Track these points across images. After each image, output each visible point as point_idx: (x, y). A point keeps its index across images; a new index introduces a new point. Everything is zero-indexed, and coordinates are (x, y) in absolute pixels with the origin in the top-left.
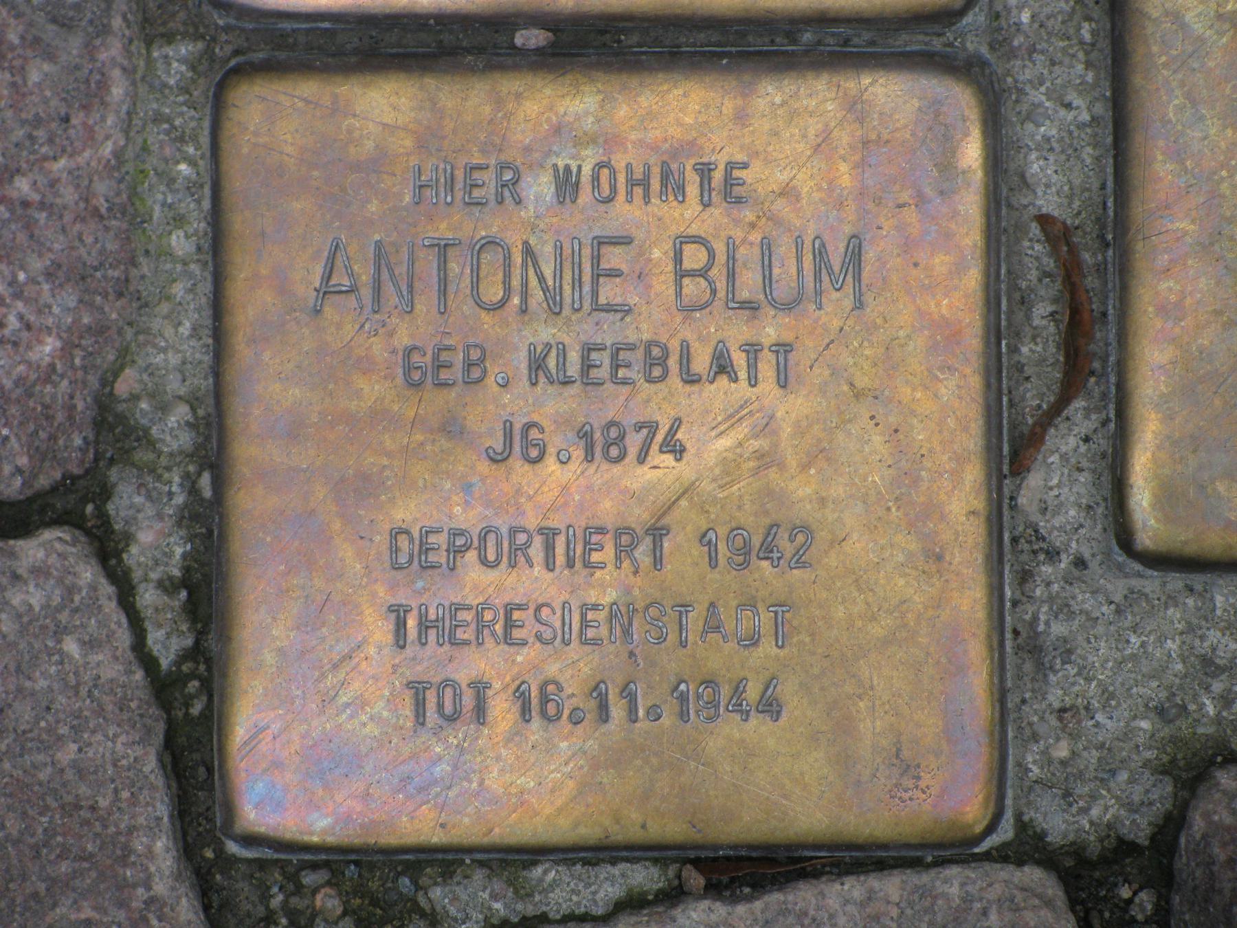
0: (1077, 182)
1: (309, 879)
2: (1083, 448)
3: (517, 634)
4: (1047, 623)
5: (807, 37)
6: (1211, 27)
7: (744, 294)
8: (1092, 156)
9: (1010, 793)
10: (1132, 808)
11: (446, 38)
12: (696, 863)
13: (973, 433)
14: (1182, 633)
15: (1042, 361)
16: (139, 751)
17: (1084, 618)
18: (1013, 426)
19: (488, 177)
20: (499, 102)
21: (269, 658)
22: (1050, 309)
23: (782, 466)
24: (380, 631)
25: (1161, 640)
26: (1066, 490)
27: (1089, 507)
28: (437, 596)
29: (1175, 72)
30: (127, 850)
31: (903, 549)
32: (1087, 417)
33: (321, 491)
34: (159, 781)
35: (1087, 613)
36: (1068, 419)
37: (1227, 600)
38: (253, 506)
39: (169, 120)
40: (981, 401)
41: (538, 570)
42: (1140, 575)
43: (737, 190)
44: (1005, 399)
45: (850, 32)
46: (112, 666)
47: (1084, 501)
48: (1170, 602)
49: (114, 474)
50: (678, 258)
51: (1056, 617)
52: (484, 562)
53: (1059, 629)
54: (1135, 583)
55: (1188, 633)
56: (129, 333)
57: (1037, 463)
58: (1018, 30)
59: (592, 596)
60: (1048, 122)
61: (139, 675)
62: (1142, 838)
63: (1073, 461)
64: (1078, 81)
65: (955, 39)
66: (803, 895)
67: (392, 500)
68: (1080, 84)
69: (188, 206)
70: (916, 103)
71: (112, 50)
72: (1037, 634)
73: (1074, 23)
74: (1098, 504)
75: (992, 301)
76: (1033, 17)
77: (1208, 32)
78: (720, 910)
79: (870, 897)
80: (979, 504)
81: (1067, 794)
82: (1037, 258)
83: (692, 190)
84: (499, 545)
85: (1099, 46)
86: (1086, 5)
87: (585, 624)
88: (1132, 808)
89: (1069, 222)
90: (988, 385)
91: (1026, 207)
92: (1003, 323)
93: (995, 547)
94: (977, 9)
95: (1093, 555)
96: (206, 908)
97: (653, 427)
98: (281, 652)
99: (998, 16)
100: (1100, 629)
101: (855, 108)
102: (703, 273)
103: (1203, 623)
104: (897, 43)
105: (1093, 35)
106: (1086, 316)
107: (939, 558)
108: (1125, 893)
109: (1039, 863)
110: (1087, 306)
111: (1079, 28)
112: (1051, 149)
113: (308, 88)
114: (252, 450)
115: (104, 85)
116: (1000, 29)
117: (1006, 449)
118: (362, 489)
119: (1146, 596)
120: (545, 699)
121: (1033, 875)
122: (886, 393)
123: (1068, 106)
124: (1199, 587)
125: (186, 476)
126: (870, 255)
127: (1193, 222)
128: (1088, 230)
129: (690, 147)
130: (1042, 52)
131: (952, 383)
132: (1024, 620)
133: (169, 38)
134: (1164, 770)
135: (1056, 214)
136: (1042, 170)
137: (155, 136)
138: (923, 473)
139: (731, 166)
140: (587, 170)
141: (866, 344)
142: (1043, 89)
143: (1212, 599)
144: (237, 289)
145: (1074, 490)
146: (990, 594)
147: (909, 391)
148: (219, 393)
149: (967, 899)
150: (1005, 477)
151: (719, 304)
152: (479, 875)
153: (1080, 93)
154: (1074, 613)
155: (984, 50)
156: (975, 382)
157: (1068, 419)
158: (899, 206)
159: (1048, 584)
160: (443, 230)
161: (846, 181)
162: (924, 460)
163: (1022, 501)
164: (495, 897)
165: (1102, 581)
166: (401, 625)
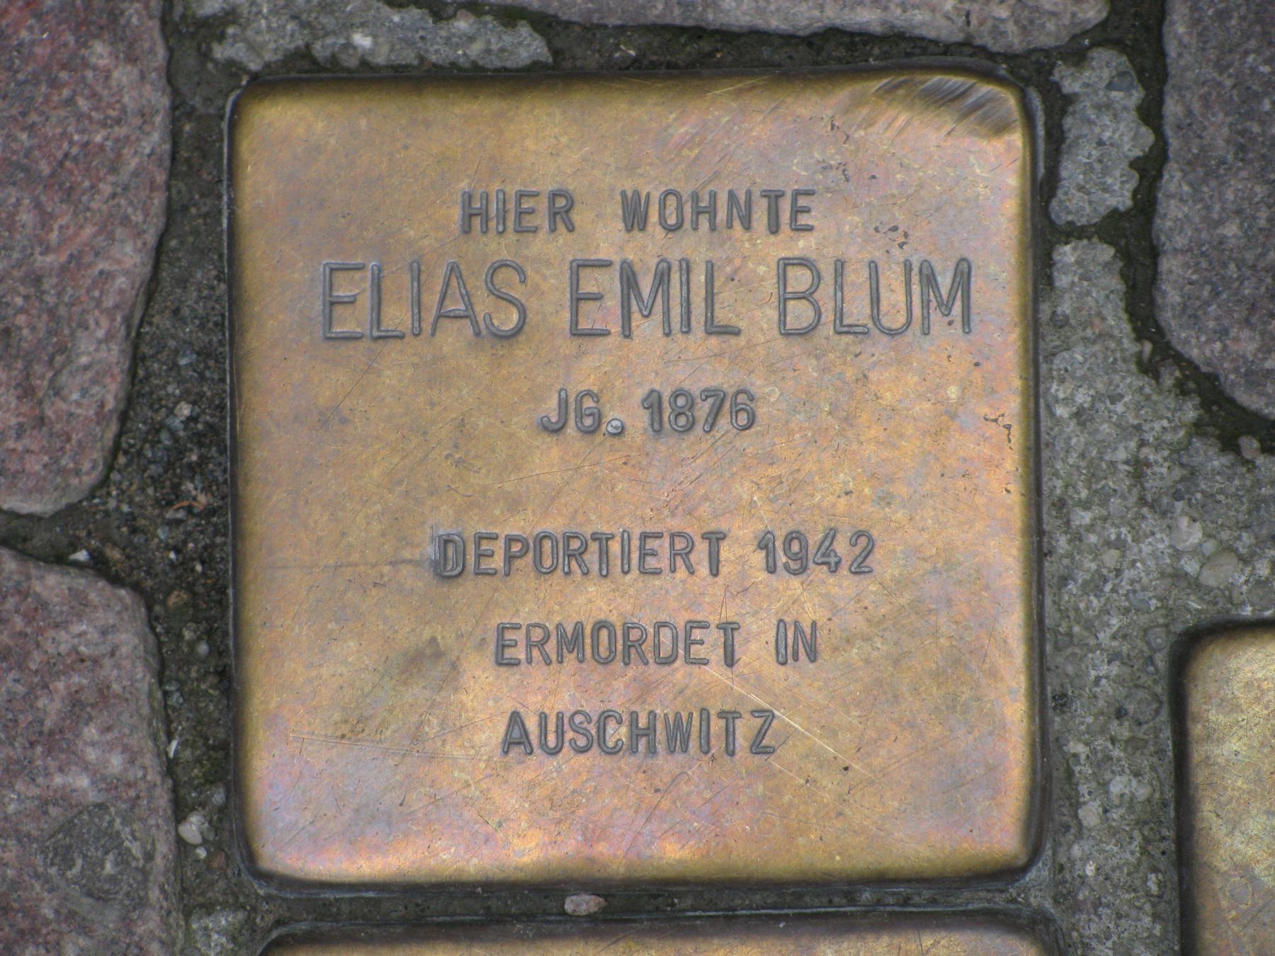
45: (909, 891)
58: (1083, 883)
64: (1145, 934)
65: (1019, 895)
68: (1148, 937)
73: (1141, 875)
94: (1040, 864)
99: (1061, 868)
104: (959, 901)
111: (1146, 880)
130: (1108, 906)
142: (1109, 944)
155: (1048, 904)
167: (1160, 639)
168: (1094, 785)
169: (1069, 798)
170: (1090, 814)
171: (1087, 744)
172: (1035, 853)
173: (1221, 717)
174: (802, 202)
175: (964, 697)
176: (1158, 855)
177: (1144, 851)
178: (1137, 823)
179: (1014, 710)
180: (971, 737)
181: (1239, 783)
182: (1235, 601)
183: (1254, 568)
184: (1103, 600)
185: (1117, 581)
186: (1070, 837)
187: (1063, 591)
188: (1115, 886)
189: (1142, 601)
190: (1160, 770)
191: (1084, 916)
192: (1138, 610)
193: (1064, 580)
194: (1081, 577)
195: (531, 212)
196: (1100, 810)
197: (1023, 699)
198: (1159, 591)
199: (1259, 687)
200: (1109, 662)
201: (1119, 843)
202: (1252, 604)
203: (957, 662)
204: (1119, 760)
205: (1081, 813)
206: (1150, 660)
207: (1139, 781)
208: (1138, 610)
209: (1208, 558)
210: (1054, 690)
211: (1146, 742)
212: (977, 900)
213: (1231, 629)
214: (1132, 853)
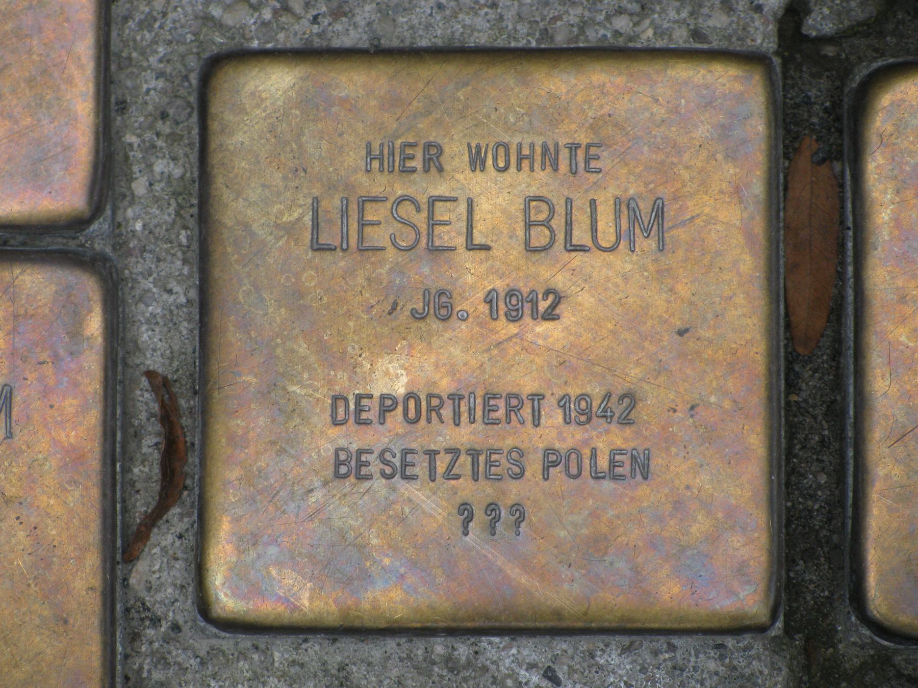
0: (176, 348)
2: (178, 543)
4: (149, 671)
6: (271, 234)
8: (187, 328)
13: (92, 530)
14: (249, 680)
15: (149, 478)
17: (177, 668)
18: (125, 526)
22: (155, 440)
26: (166, 573)
27: (182, 587)
29: (244, 266)
31: (40, 615)
32: (181, 520)
35: (179, 664)
36: (167, 521)
37: (283, 655)
40: (98, 506)
42: (216, 636)
44: (118, 506)
45: (7, 235)
47: (179, 582)
48: (241, 657)
51: (155, 667)
54: (214, 642)
55: (254, 680)
57: (144, 554)
58: (134, 236)
60: (154, 303)
63: (171, 552)
64: (177, 273)
65: (86, 242)
68: (179, 275)
70: (54, 287)
72: (142, 680)
73: (175, 231)
74: (189, 584)
76: (144, 226)
77: (269, 238)
80: (97, 582)
82: (146, 403)
85: (192, 248)
86: (184, 218)
89: (170, 377)
90: (104, 495)
91: (138, 366)
92: (118, 450)
93: (108, 613)
94: (101, 220)
95: (186, 622)
99: (119, 225)
100: (189, 676)
103: (265, 672)
104: (42, 244)
105: (188, 240)
106: (181, 446)
107: (66, 622)
110: (181, 438)
111: (178, 235)
112: (157, 323)
116: (121, 235)
117: (119, 543)
119: (223, 652)
122: (29, 500)
123: (170, 292)
124: (262, 646)
126: (18, 399)
127: (255, 376)
128: (184, 382)
130: (151, 252)
131: (77, 494)
132: (133, 670)
135: (160, 371)
136: (150, 338)
138: (55, 559)
141: (14, 464)
142: (151, 279)
143: (272, 655)
145: (172, 574)
146: (104, 649)
147: (45, 498)
150: (118, 563)
153: (179, 282)
154: (169, 664)
155: (108, 250)
156: (95, 492)
157: (167, 521)
158: (40, 363)
159: (151, 643)
162: (56, 550)
163: (133, 581)
165: (191, 641)
167: (193, 62)
168: (143, 165)
169: (126, 176)
170: (140, 187)
171: (139, 136)
172: (96, 210)
173: (231, 117)
174: (593, 151)
175: (48, 97)
176: (188, 217)
177: (178, 214)
178: (174, 194)
179: (82, 105)
180: (52, 125)
181: (243, 164)
182: (247, 37)
183: (260, 14)
184: (153, 34)
185: (163, 21)
186: (126, 203)
187: (126, 26)
188: (157, 239)
189: (181, 35)
190: (191, 157)
191: (133, 259)
192: (178, 42)
193: (126, 19)
194: (138, 17)
195: (412, 158)
196: (147, 183)
197: (90, 100)
198: (192, 29)
199: (259, 96)
200: (157, 78)
201: (161, 208)
202: (258, 39)
203: (44, 72)
204: (161, 148)
205: (133, 185)
206: (186, 78)
207: (175, 164)
208: (178, 42)
209: (229, 6)
210: (117, 98)
211: (182, 136)
212: (55, 243)
213: (243, 56)
214: (169, 215)
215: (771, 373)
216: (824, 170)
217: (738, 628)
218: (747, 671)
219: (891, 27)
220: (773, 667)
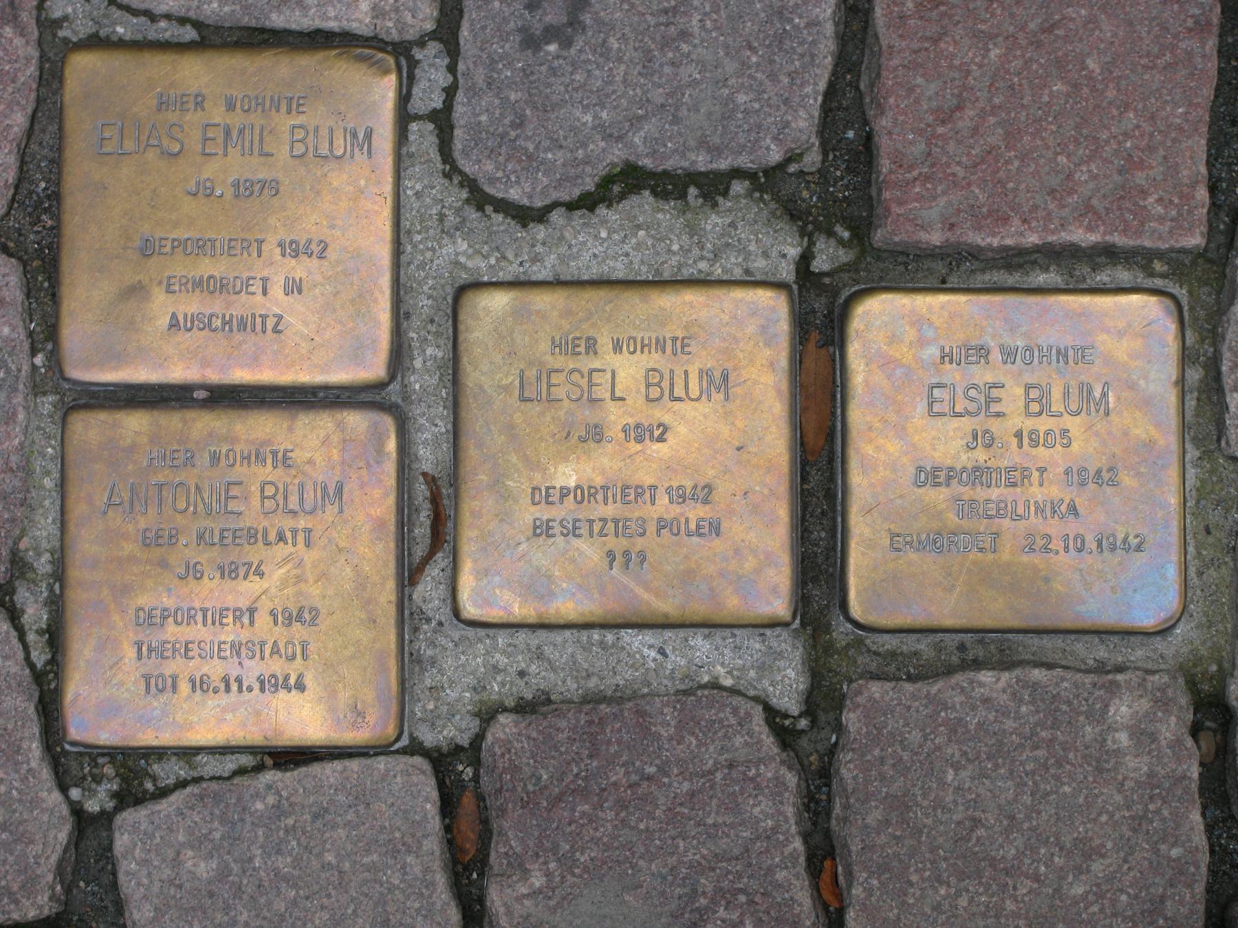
1: (101, 760)
3: (190, 654)
5: (321, 394)
7: (291, 506)
9: (406, 724)
10: (461, 731)
11: (165, 394)
12: (271, 754)
16: (27, 704)
18: (410, 564)
19: (181, 454)
20: (185, 422)
21: (82, 664)
23: (306, 581)
24: (131, 653)
25: (475, 657)
28: (156, 637)
30: (19, 748)
33: (106, 592)
34: (35, 718)
38: (77, 598)
39: (43, 429)
41: (200, 625)
43: (289, 462)
46: (15, 667)
49: (17, 583)
50: (262, 491)
52: (176, 622)
53: (429, 652)
56: (26, 522)
59: (223, 638)
61: (27, 671)
62: (466, 744)
66: (316, 769)
67: (136, 595)
69: (51, 466)
71: (19, 399)
75: (400, 510)
78: (279, 774)
79: (345, 769)
80: (393, 598)
81: (433, 724)
83: (269, 461)
84: (183, 615)
87: (220, 650)
88: (461, 731)
90: (397, 547)
96: (56, 773)
97: (250, 565)
98: (87, 661)
101: (340, 426)
102: (273, 497)
107: (375, 621)
108: (460, 768)
109: (421, 755)
113: (103, 416)
114: (75, 573)
115: (15, 414)
118: (127, 590)
120: (202, 682)
121: (418, 760)
125: (49, 584)
126: (346, 490)
129: (268, 442)
133: (44, 394)
134: (477, 715)
137: (37, 436)
139: (286, 451)
140: (224, 451)
144: (70, 503)
148: (62, 548)
149: (387, 771)
151: (280, 511)
152: (174, 759)
155: (399, 401)
156: (392, 545)
160: (161, 478)
161: (336, 457)
163: (414, 597)
164: (180, 769)
166: (140, 649)
215: (792, 473)
216: (823, 351)
217: (774, 624)
218: (779, 650)
219: (863, 266)
220: (794, 646)
